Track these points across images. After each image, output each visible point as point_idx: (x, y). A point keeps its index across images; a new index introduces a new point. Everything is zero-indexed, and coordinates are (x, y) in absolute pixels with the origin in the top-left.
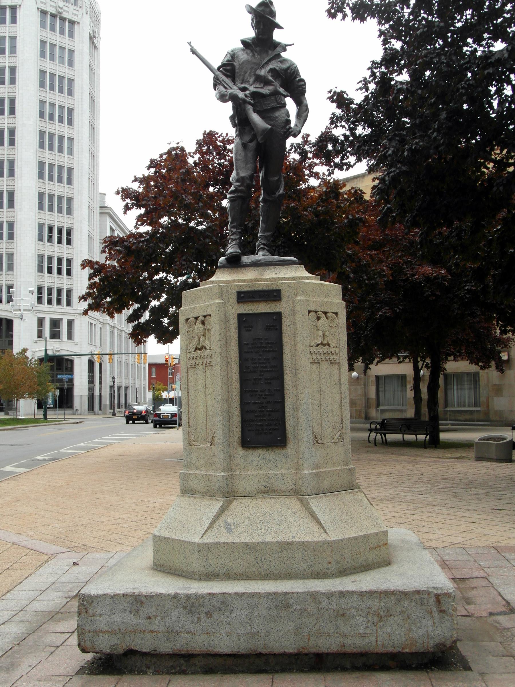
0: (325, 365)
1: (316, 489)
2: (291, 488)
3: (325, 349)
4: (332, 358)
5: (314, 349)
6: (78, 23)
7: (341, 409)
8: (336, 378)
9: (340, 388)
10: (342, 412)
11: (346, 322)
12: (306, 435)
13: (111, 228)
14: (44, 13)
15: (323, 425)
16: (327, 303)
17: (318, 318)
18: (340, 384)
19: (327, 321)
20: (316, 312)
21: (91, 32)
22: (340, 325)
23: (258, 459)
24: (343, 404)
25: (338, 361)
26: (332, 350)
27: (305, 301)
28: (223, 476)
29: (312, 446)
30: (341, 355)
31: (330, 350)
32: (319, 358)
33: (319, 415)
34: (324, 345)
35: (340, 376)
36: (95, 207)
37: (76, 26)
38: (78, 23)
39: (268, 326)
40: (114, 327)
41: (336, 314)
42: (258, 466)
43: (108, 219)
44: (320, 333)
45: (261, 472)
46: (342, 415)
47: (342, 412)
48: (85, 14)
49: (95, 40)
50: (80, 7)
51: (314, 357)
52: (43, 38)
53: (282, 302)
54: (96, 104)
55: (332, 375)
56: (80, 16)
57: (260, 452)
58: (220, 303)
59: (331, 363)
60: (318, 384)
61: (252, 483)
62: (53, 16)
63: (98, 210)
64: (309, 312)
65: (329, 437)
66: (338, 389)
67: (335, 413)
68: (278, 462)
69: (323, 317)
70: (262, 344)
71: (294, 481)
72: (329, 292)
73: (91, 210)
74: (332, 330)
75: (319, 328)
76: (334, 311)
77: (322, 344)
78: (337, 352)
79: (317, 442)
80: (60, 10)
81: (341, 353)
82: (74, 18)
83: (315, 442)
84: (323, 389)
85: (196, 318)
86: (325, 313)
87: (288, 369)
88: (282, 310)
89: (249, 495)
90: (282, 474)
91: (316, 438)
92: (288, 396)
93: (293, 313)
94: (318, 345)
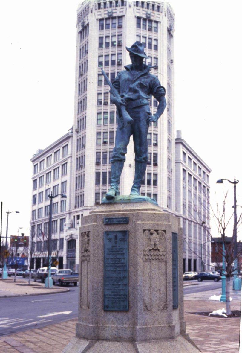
0: (155, 263)
1: (144, 338)
2: (130, 336)
3: (155, 253)
4: (160, 258)
5: (147, 253)
6: (160, 22)
7: (167, 289)
8: (163, 270)
9: (166, 276)
10: (166, 291)
11: (171, 236)
12: (140, 305)
13: (184, 153)
14: (139, 18)
15: (153, 299)
16: (158, 225)
17: (151, 234)
18: (166, 274)
19: (157, 236)
20: (149, 230)
21: (169, 27)
22: (167, 238)
23: (113, 318)
24: (167, 287)
25: (165, 260)
26: (161, 253)
27: (141, 224)
28: (91, 327)
29: (143, 311)
30: (167, 256)
31: (159, 253)
32: (150, 258)
33: (150, 293)
34: (155, 250)
35: (166, 269)
36: (172, 139)
37: (159, 24)
38: (160, 22)
39: (121, 239)
40: (191, 221)
41: (165, 231)
42: (113, 323)
43: (181, 146)
44: (152, 243)
45: (113, 326)
46: (166, 293)
47: (166, 291)
48: (164, 16)
49: (171, 32)
50: (161, 12)
51: (147, 257)
52: (138, 34)
53: (129, 225)
54: (172, 72)
55: (160, 268)
56: (161, 18)
57: (114, 314)
58: (94, 225)
59: (159, 261)
60: (150, 274)
61: (108, 332)
62: (145, 20)
63: (174, 142)
64: (144, 230)
65: (157, 306)
66: (165, 277)
67: (161, 292)
68: (123, 320)
69: (155, 233)
70: (116, 249)
71: (132, 332)
72: (160, 218)
73: (169, 141)
74: (161, 241)
75: (152, 240)
76: (162, 229)
77: (153, 249)
78: (164, 254)
79: (147, 309)
80: (149, 16)
81: (167, 255)
82: (157, 20)
83: (145, 309)
84: (153, 277)
85: (85, 233)
86: (157, 231)
87: (131, 264)
88: (129, 229)
89: (107, 340)
90: (125, 327)
91: (146, 306)
92: (131, 281)
93: (136, 230)
94: (150, 250)
